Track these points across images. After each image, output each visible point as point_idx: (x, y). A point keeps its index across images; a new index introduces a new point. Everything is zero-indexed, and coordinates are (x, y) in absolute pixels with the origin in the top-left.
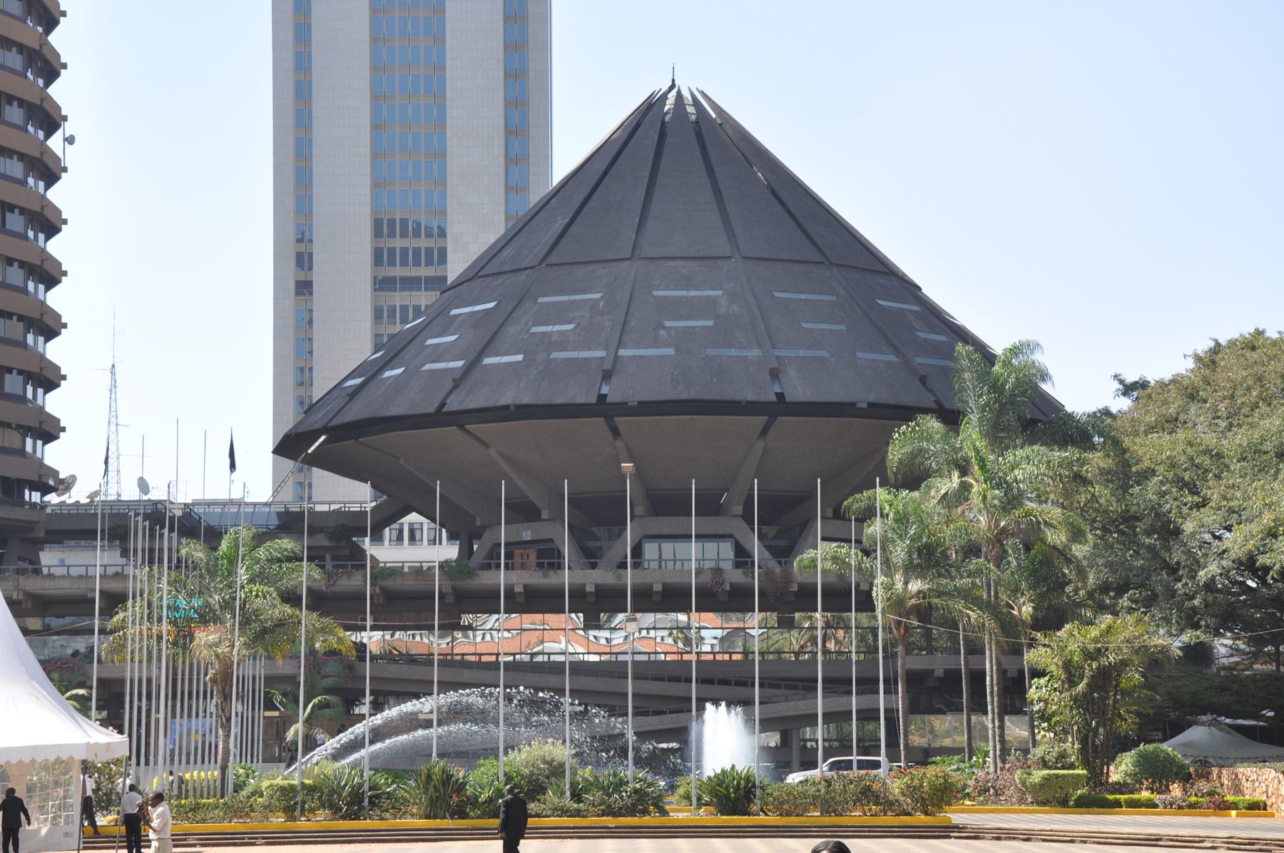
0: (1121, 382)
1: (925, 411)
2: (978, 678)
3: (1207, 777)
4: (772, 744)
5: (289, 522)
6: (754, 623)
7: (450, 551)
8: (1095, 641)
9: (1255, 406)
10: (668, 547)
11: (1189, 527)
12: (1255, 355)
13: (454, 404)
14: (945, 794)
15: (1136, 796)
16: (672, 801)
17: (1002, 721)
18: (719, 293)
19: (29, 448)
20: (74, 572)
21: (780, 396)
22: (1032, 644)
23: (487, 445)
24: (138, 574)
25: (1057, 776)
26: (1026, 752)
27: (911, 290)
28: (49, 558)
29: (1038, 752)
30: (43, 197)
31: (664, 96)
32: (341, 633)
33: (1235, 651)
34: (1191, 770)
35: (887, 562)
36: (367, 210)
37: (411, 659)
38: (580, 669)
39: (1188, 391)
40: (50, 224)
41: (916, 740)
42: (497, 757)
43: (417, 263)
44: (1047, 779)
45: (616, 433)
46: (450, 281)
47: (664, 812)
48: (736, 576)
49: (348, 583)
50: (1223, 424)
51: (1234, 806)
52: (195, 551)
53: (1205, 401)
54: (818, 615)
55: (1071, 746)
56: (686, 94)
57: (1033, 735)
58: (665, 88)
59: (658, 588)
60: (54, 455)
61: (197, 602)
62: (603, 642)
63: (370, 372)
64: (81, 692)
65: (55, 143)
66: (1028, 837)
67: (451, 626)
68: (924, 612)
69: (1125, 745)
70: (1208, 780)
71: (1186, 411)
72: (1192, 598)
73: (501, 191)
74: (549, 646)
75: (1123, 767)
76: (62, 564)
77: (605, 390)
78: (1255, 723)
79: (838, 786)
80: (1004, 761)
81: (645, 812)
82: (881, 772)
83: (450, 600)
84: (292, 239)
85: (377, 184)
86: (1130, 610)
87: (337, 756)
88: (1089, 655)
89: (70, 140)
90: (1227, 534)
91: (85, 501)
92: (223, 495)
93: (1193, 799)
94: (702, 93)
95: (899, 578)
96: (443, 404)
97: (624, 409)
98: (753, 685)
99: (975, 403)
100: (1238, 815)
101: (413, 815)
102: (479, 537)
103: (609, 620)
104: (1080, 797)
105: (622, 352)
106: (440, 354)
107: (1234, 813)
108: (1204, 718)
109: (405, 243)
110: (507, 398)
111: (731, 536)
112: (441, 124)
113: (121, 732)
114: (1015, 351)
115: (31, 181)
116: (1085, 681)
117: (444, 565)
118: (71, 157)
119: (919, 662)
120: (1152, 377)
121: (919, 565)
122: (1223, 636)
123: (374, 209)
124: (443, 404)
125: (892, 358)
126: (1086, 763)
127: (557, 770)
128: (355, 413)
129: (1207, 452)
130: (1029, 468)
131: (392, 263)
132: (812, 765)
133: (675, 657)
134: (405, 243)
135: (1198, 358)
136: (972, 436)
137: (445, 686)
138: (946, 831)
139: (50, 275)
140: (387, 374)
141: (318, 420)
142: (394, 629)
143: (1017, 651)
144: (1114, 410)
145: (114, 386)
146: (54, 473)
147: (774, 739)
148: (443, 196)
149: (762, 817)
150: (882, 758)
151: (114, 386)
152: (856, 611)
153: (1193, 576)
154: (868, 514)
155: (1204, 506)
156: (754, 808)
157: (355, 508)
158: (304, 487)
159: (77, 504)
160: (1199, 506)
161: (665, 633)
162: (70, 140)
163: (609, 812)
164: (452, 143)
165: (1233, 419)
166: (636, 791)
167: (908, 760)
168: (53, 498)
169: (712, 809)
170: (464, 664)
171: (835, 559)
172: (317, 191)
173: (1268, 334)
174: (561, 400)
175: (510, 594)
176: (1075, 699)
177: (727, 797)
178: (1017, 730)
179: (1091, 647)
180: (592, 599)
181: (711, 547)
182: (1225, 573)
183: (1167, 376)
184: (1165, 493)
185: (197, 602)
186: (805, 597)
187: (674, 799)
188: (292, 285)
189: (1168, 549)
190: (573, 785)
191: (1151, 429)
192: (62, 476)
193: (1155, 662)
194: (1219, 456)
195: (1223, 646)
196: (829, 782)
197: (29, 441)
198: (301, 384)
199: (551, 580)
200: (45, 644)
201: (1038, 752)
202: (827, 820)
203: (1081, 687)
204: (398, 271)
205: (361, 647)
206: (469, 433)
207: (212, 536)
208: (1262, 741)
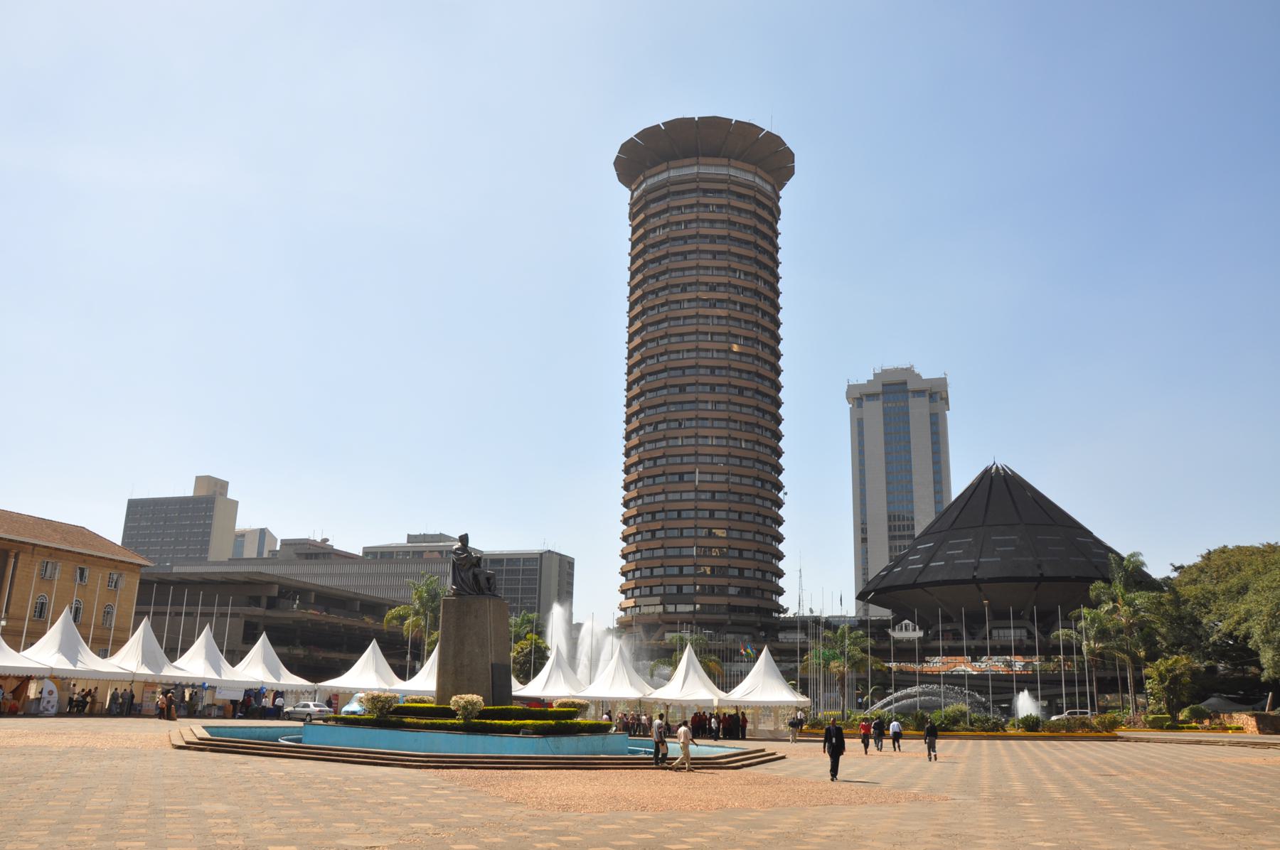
0: (1174, 566)
1: (1098, 579)
2: (1124, 680)
3: (1218, 717)
4: (1045, 705)
5: (862, 624)
6: (1037, 661)
7: (920, 634)
8: (1171, 665)
9: (1227, 574)
10: (1001, 632)
11: (1205, 621)
12: (1225, 555)
13: (920, 580)
14: (1114, 724)
15: (1190, 725)
16: (1008, 727)
17: (1135, 696)
18: (1016, 537)
19: (774, 598)
20: (790, 641)
21: (1042, 575)
22: (1146, 667)
24: (811, 642)
25: (1158, 717)
26: (1145, 708)
27: (1088, 534)
28: (781, 636)
29: (1150, 708)
30: (777, 513)
31: (991, 468)
32: (882, 663)
33: (1226, 668)
34: (1212, 715)
35: (1087, 637)
36: (885, 512)
37: (907, 673)
38: (971, 676)
39: (1199, 569)
40: (779, 521)
41: (1101, 703)
42: (941, 709)
43: (904, 530)
44: (1154, 719)
45: (980, 589)
46: (916, 536)
47: (1005, 731)
48: (1028, 642)
49: (885, 645)
50: (1215, 581)
51: (1230, 729)
52: (829, 634)
53: (1207, 573)
54: (1061, 657)
55: (1163, 705)
56: (999, 466)
57: (1148, 702)
58: (992, 464)
59: (998, 647)
60: (782, 601)
61: (831, 652)
62: (978, 666)
63: (889, 569)
64: (793, 682)
65: (781, 495)
66: (1148, 741)
67: (922, 661)
68: (1101, 655)
69: (1184, 705)
70: (1219, 718)
71: (1200, 577)
72: (1208, 648)
73: (933, 503)
74: (958, 668)
75: (1184, 714)
76: (785, 638)
77: (975, 574)
78: (1235, 696)
79: (1072, 721)
80: (1137, 712)
81: (998, 731)
82: (1089, 715)
83: (921, 651)
85: (889, 503)
86: (1183, 653)
87: (882, 707)
88: (1168, 671)
89: (786, 494)
90: (1220, 624)
91: (792, 616)
92: (838, 614)
93: (1214, 726)
94: (1006, 466)
95: (1092, 642)
96: (916, 581)
97: (983, 581)
98: (1037, 683)
99: (1118, 576)
100: (1232, 732)
101: (911, 730)
102: (930, 629)
103: (980, 659)
104: (1168, 725)
105: (981, 560)
106: (914, 562)
107: (1230, 731)
108: (1215, 694)
109: (900, 523)
110: (939, 578)
111: (1025, 627)
112: (911, 481)
113: (808, 697)
114: (1132, 555)
115: (773, 508)
116: (1168, 681)
117: (919, 638)
118: (786, 499)
119: (1102, 674)
120: (1186, 564)
121: (1100, 637)
122: (1221, 663)
123: (888, 512)
124: (916, 581)
125: (1084, 559)
126: (1170, 713)
127: (963, 714)
128: (884, 584)
129: (1210, 592)
130: (1141, 600)
132: (1060, 712)
133: (1006, 673)
134: (900, 523)
135: (1203, 557)
136: (1118, 588)
137: (921, 683)
138: (1115, 738)
139: (780, 539)
140: (895, 570)
141: (871, 587)
142: (900, 662)
143: (1139, 669)
144: (1172, 577)
145: (801, 577)
146: (782, 607)
147: (1045, 703)
148: (912, 506)
149: (1043, 733)
150: (1089, 711)
151: (801, 577)
152: (1076, 654)
153: (1208, 639)
154: (1079, 618)
155: (1210, 613)
156: (1040, 729)
157: (885, 618)
158: (866, 611)
159: (790, 617)
160: (1208, 613)
161: (1001, 663)
162: (786, 494)
163: (984, 730)
164: (915, 487)
165: (1219, 579)
166: (994, 723)
167: (1099, 711)
168: (782, 615)
169: (1023, 729)
170: (926, 675)
171: (1067, 635)
172: (868, 506)
173: (1229, 547)
176: (1164, 688)
177: (1029, 725)
178: (1141, 700)
179: (1169, 668)
181: (1018, 631)
182: (1220, 639)
183: (1191, 564)
184: (1195, 608)
185: (831, 652)
186: (1056, 650)
187: (1008, 725)
188: (860, 539)
189: (1197, 630)
190: (970, 720)
191: (1187, 584)
192: (785, 608)
193: (1195, 673)
194: (1215, 594)
195: (1221, 666)
196: (1068, 720)
197: (774, 596)
198: (108, 613)
199: (958, 644)
200: (781, 665)
201: (1150, 708)
202: (1068, 734)
203: (1166, 683)
204: (897, 533)
205: (890, 669)
206: (925, 590)
207: (835, 628)
208: (1239, 703)
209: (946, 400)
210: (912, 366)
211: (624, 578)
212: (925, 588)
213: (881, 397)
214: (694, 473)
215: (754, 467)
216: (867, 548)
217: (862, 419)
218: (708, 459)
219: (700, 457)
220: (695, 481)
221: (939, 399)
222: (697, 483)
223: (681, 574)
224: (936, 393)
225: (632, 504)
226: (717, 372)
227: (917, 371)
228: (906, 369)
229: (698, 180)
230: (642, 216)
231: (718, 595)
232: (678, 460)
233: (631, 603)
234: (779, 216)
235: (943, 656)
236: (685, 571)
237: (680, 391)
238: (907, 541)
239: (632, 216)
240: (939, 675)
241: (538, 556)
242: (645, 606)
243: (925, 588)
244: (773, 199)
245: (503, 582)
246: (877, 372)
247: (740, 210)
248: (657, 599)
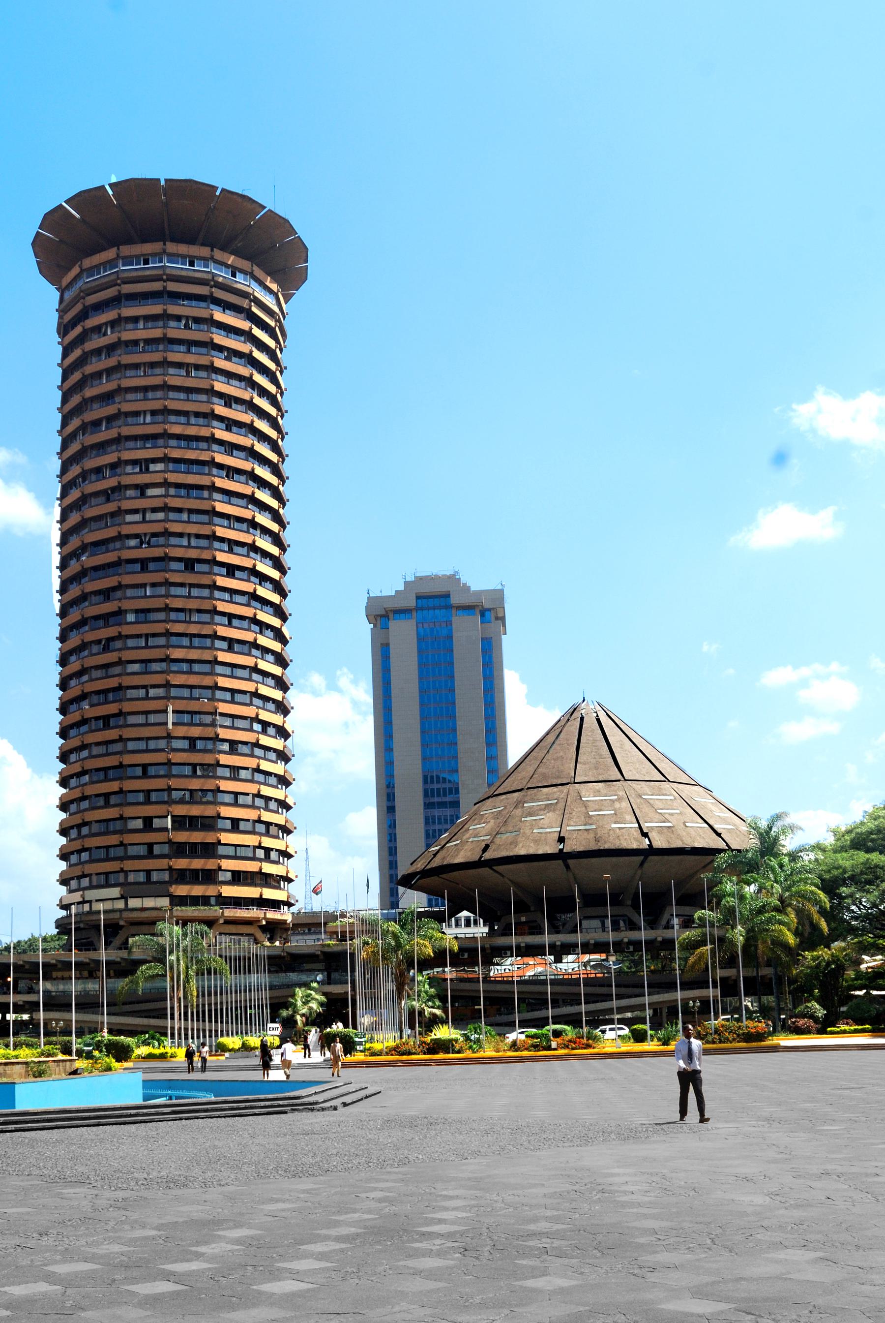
23: (503, 876)
43: (445, 795)
45: (568, 867)
62: (507, 971)
84: (385, 786)
85: (424, 759)
109: (439, 786)
123: (424, 771)
124: (481, 857)
131: (433, 796)
134: (439, 786)
174: (540, 852)
175: (583, 945)
180: (559, 949)
188: (385, 808)
204: (436, 799)
209: (503, 619)
211: (64, 863)
212: (495, 868)
213: (414, 613)
214: (165, 711)
215: (251, 704)
216: (395, 821)
217: (387, 645)
218: (186, 693)
219: (172, 690)
220: (166, 724)
222: (170, 726)
223: (150, 855)
224: (489, 610)
225: (73, 757)
227: (463, 580)
229: (165, 277)
230: (78, 330)
232: (142, 693)
233: (77, 897)
235: (517, 956)
236: (157, 850)
237: (186, 568)
238: (436, 810)
239: (63, 329)
240: (544, 982)
242: (97, 901)
243: (495, 868)
248: (115, 892)
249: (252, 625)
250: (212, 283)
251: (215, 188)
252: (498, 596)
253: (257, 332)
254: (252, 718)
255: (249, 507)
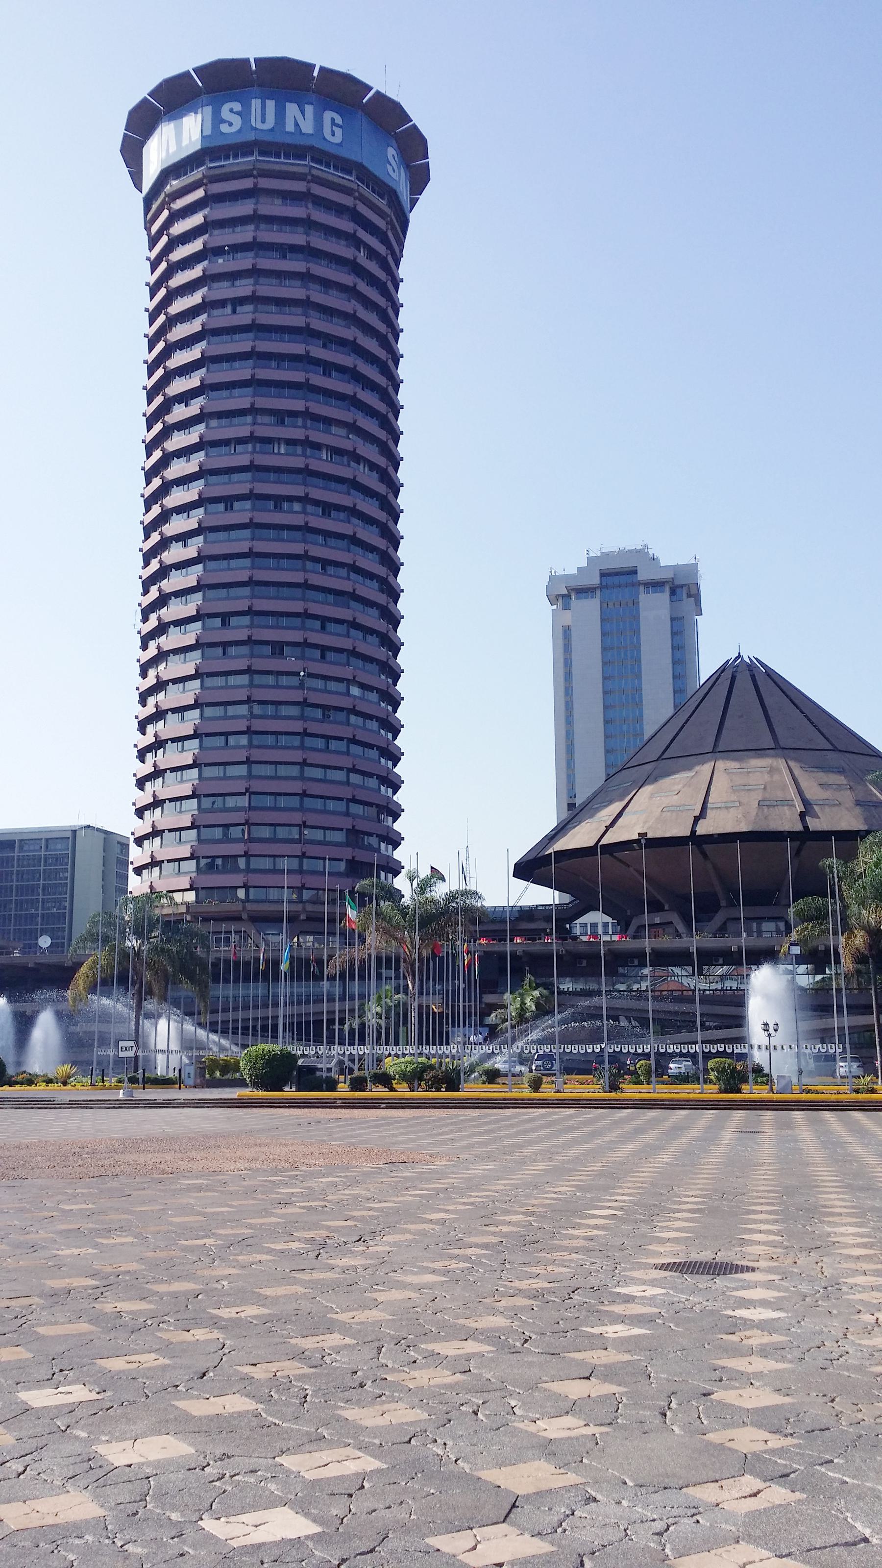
94: (756, 659)
188: (566, 806)
206: (615, 857)
210: (646, 546)
213: (598, 592)
221: (685, 596)
224: (682, 586)
226: (285, 506)
228: (638, 551)
229: (255, 172)
231: (224, 871)
234: (401, 251)
241: (69, 834)
244: (388, 216)
245: (14, 877)
246: (592, 554)
247: (327, 284)
249: (351, 574)
250: (309, 178)
251: (311, 67)
252: (692, 570)
253: (363, 287)
254: (348, 680)
255: (350, 436)
